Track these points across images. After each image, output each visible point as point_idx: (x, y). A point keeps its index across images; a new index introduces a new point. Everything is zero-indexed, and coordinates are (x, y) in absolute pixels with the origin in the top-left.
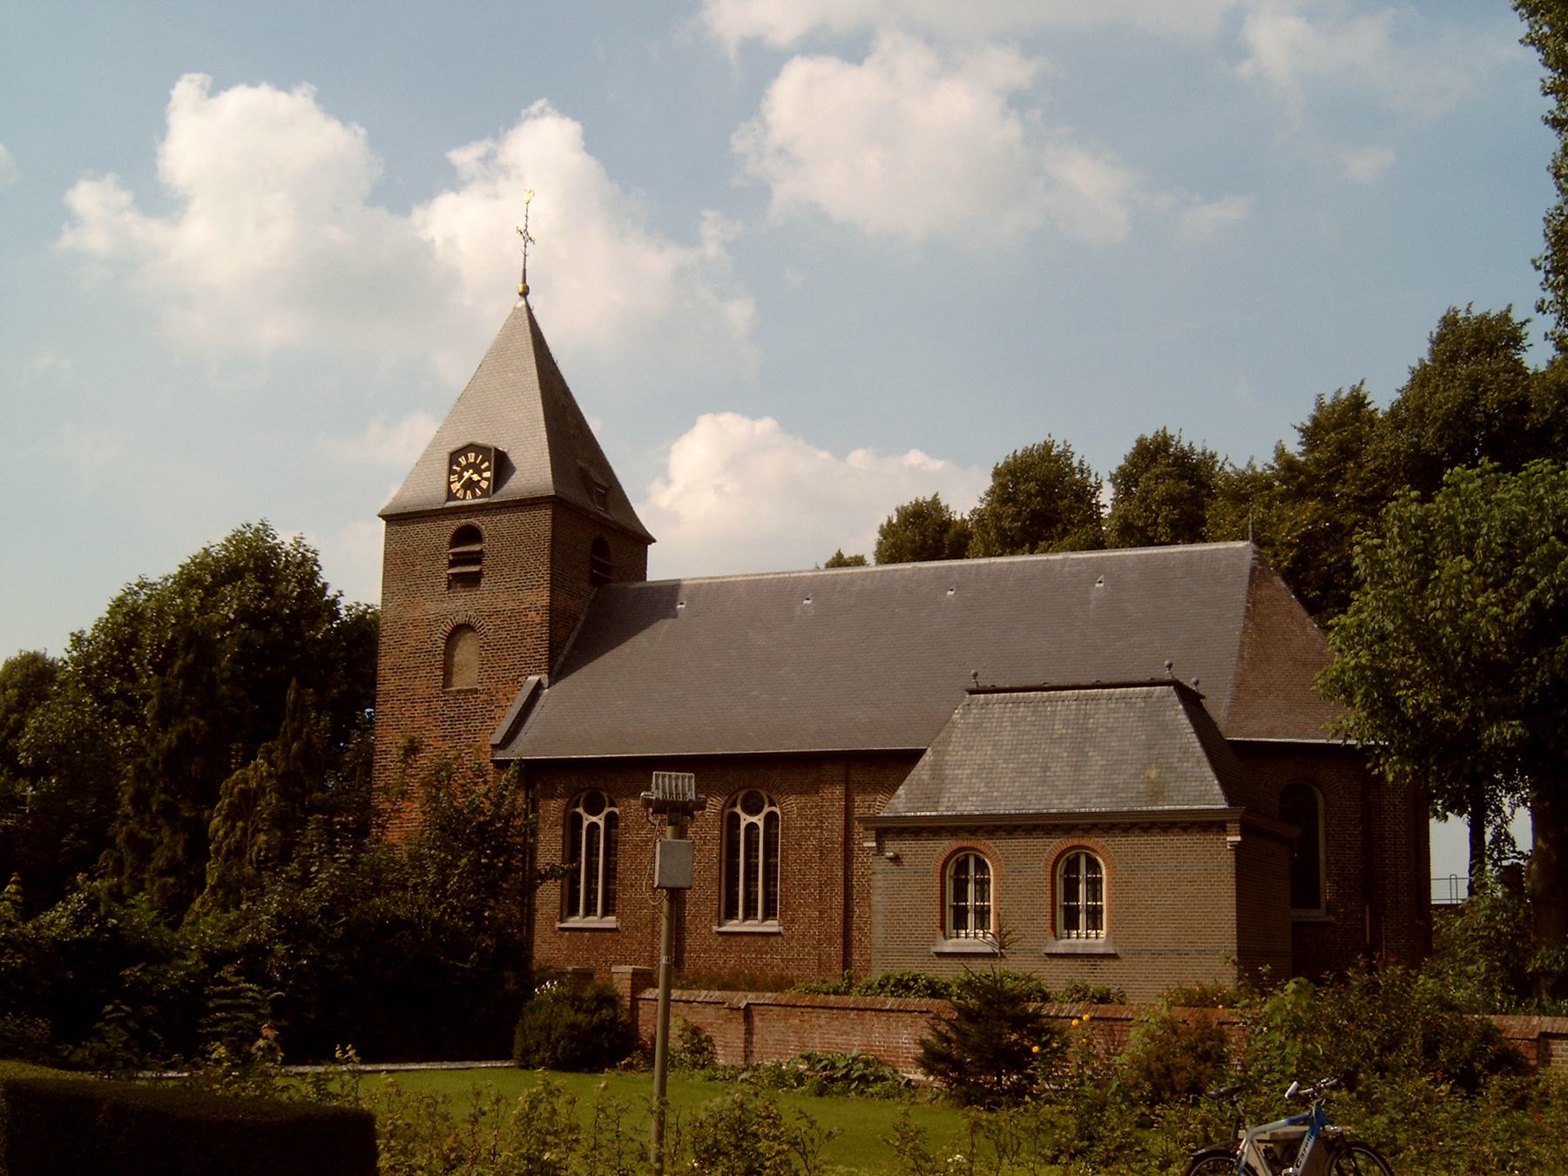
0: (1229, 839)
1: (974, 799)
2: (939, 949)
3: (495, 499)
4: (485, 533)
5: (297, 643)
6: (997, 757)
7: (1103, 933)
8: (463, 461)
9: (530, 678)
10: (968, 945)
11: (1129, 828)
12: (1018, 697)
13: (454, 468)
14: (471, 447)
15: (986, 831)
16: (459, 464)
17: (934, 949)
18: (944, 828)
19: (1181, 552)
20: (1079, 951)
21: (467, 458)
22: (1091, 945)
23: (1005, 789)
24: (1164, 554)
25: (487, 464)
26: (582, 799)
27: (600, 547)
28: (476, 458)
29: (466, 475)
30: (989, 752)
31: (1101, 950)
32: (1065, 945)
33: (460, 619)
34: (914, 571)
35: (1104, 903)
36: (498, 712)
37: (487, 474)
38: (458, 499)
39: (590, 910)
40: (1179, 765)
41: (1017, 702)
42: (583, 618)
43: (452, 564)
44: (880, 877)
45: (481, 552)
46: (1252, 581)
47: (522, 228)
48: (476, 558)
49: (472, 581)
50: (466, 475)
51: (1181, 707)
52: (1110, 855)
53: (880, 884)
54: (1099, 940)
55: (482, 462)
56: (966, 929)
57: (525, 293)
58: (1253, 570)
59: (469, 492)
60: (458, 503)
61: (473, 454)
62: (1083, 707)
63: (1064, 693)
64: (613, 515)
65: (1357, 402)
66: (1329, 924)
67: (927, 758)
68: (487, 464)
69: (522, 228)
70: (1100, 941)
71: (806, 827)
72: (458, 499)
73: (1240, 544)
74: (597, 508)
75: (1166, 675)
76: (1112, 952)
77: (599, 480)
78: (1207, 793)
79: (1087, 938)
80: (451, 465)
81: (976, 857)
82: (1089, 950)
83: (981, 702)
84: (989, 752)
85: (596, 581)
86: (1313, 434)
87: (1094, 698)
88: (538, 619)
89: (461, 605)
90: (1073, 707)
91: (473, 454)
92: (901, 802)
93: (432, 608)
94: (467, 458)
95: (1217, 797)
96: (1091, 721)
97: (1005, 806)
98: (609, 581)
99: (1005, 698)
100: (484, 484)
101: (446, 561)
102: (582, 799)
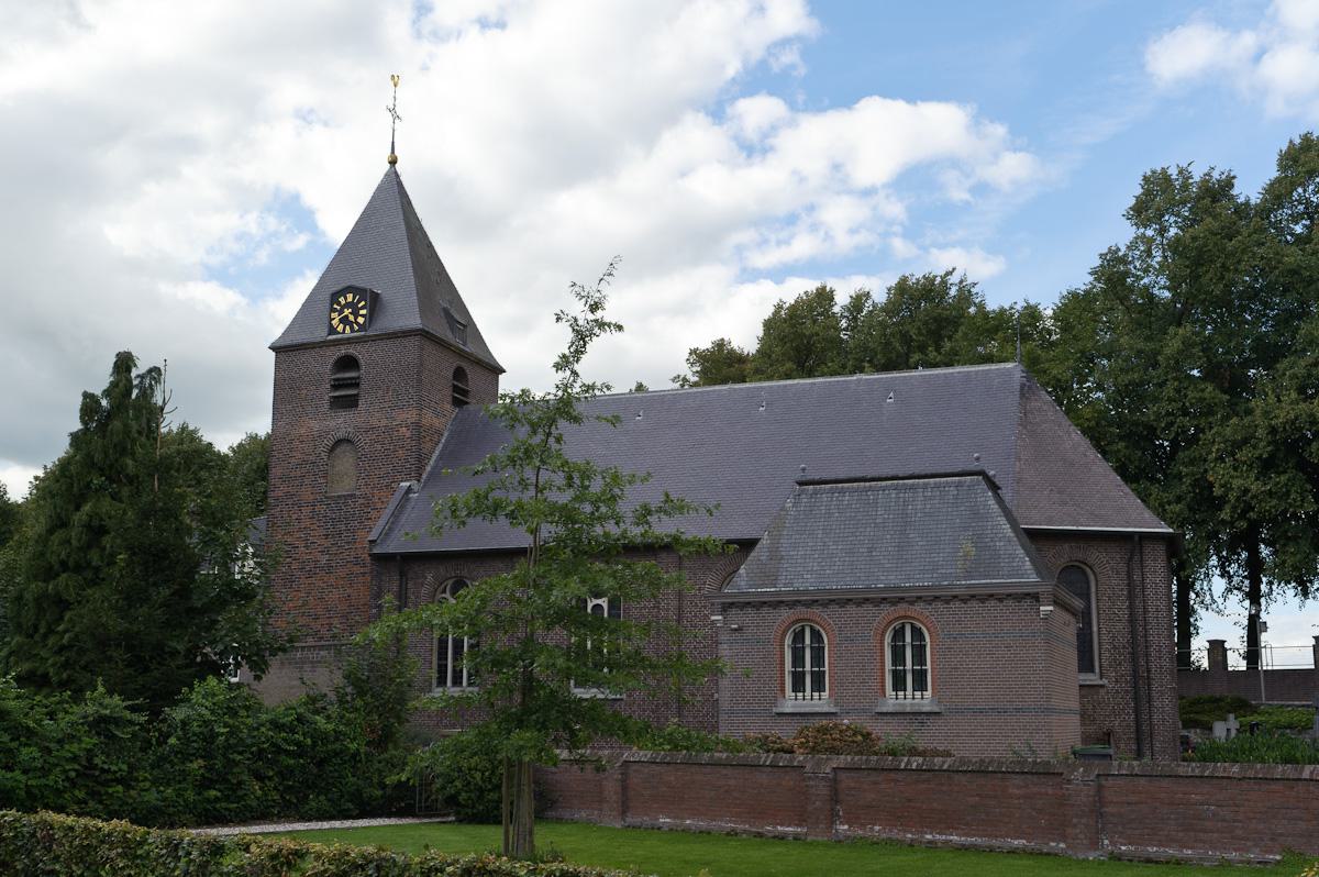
0: (1042, 608)
1: (809, 576)
2: (780, 710)
3: (370, 333)
4: (362, 362)
5: (368, 808)
6: (827, 540)
7: (928, 694)
8: (342, 300)
9: (402, 484)
10: (805, 706)
11: (915, 602)
12: (842, 488)
13: (335, 306)
14: (350, 289)
15: (821, 605)
16: (339, 303)
17: (774, 710)
18: (782, 602)
19: (959, 373)
20: (908, 710)
21: (346, 299)
22: (918, 705)
23: (836, 568)
24: (945, 374)
25: (363, 303)
26: (448, 587)
27: (459, 374)
28: (354, 299)
29: (347, 312)
30: (820, 536)
31: (925, 709)
32: (894, 705)
33: (341, 434)
34: (729, 391)
35: (929, 667)
36: (373, 514)
37: (363, 312)
38: (339, 333)
39: (457, 681)
40: (992, 544)
41: (842, 491)
42: (446, 434)
43: (335, 387)
44: (725, 646)
45: (358, 378)
46: (1022, 395)
47: (391, 107)
48: (355, 384)
49: (350, 403)
50: (347, 312)
51: (990, 494)
52: (830, 624)
53: (726, 652)
54: (925, 700)
55: (359, 302)
56: (804, 692)
57: (393, 162)
58: (1023, 386)
59: (348, 327)
60: (340, 336)
61: (351, 295)
62: (902, 495)
63: (884, 483)
64: (470, 348)
65: (1229, 183)
66: (1102, 686)
67: (765, 542)
68: (363, 303)
69: (391, 107)
70: (925, 701)
71: (645, 608)
72: (339, 333)
73: (1010, 365)
74: (457, 342)
75: (974, 466)
76: (938, 710)
77: (457, 317)
78: (1023, 570)
79: (913, 698)
80: (332, 305)
81: (812, 628)
82: (916, 709)
83: (811, 492)
84: (820, 536)
85: (458, 403)
86: (1282, 166)
87: (912, 487)
88: (408, 434)
89: (342, 423)
90: (893, 496)
91: (351, 295)
92: (744, 580)
93: (315, 425)
94: (346, 299)
95: (1029, 572)
96: (910, 507)
97: (837, 583)
98: (467, 403)
99: (832, 488)
100: (361, 320)
101: (328, 386)
102: (448, 587)
